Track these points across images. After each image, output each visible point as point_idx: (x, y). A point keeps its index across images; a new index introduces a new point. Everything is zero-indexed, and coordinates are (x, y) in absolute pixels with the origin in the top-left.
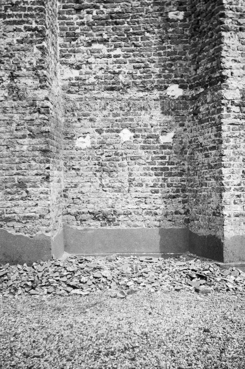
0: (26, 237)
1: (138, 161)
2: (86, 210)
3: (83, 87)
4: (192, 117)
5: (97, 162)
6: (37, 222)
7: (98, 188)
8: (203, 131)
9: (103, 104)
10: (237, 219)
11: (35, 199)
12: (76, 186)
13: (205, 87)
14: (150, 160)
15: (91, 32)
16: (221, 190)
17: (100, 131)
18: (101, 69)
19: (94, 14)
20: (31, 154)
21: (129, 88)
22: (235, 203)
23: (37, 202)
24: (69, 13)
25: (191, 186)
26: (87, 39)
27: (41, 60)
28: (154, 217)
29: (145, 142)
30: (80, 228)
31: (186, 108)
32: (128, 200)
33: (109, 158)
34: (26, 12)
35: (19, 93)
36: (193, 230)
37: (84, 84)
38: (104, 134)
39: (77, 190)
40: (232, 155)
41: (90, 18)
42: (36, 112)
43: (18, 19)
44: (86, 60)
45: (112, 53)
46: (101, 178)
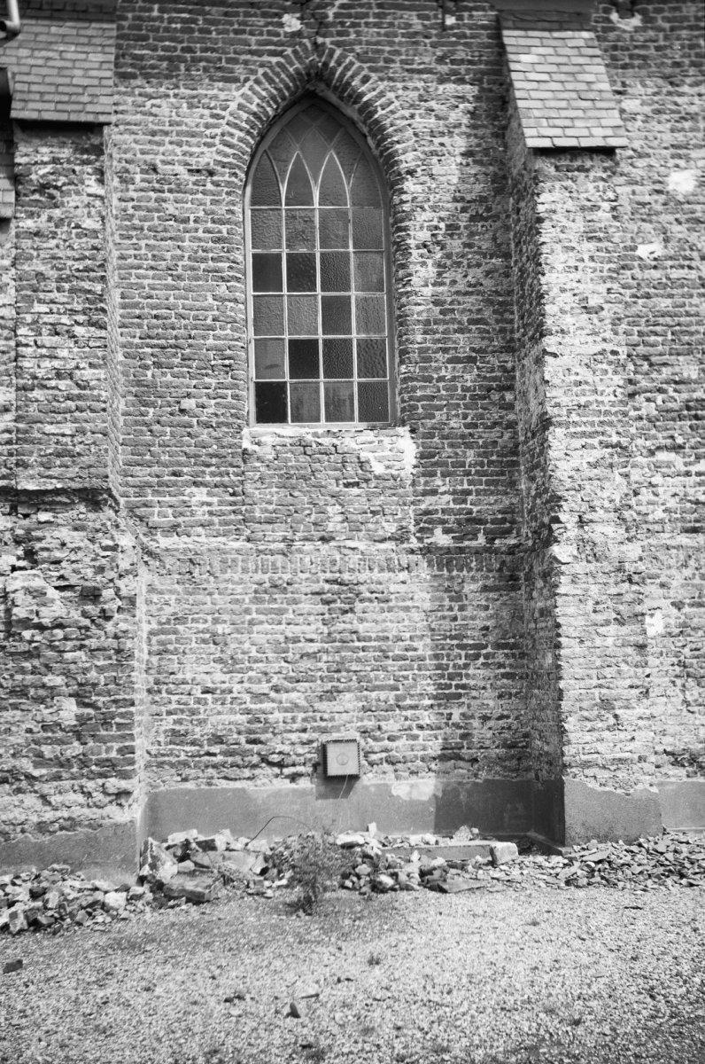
0: (619, 795)
3: (644, 526)
5: (675, 660)
6: (635, 767)
7: (679, 708)
9: (682, 557)
11: (629, 728)
15: (653, 432)
17: (678, 605)
18: (675, 495)
20: (620, 652)
23: (635, 734)
26: (648, 443)
33: (697, 653)
34: (602, 419)
37: (646, 522)
38: (686, 609)
42: (624, 581)
43: (589, 429)
44: (649, 480)
45: (694, 469)
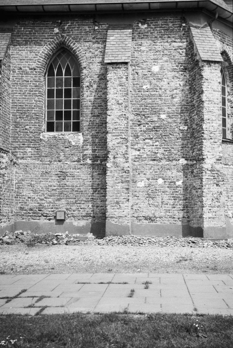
1: (166, 193)
2: (141, 215)
3: (141, 159)
4: (191, 174)
5: (147, 193)
6: (124, 218)
8: (195, 181)
10: (209, 219)
11: (123, 209)
12: (137, 204)
13: (197, 161)
14: (171, 193)
15: (145, 134)
16: (203, 207)
17: (148, 179)
18: (149, 151)
19: (147, 127)
20: (122, 190)
21: (162, 159)
22: (209, 213)
24: (135, 126)
25: (190, 205)
26: (143, 137)
27: (126, 151)
28: (173, 219)
29: (169, 184)
30: (138, 223)
31: (188, 169)
32: (161, 211)
33: (152, 191)
34: (121, 132)
35: (117, 164)
36: (191, 225)
38: (150, 180)
39: (137, 206)
40: (207, 192)
41: (144, 129)
43: (117, 134)
45: (155, 144)
46: (149, 201)
